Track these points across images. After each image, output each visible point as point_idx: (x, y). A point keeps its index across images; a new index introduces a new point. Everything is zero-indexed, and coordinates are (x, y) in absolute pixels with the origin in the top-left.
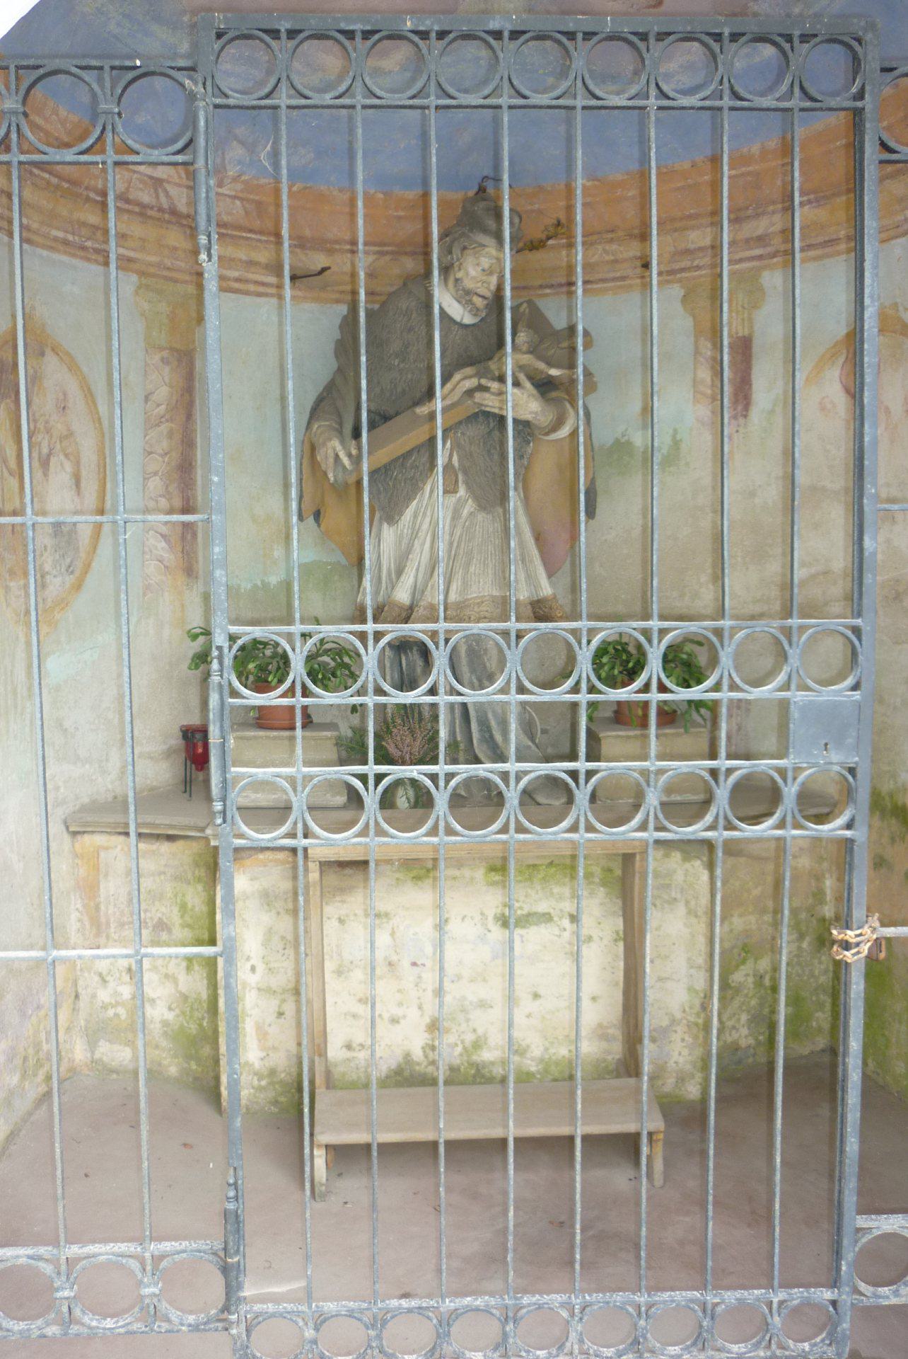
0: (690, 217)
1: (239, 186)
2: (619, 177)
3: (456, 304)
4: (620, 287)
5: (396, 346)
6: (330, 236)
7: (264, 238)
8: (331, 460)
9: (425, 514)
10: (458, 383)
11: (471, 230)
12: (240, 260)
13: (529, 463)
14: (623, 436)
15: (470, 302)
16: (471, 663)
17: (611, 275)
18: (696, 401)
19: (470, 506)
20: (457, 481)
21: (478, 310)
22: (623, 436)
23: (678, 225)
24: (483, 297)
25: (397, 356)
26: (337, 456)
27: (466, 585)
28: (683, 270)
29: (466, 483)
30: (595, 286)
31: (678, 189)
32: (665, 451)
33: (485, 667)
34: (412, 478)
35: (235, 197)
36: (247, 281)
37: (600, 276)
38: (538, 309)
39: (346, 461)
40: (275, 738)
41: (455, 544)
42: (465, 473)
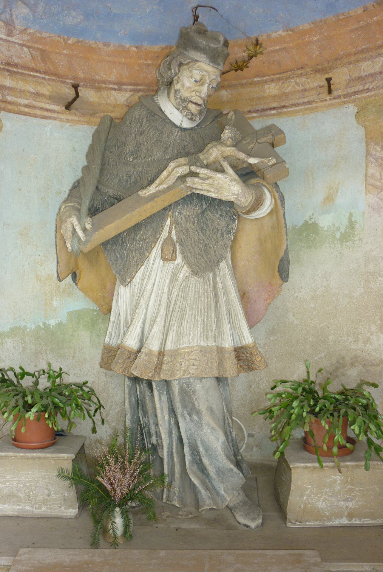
0: (362, 51)
1: (26, 37)
2: (307, 26)
3: (177, 112)
5: (130, 147)
6: (98, 77)
7: (47, 77)
8: (70, 233)
9: (149, 276)
10: (173, 170)
11: (186, 49)
12: (29, 92)
13: (235, 237)
14: (311, 219)
16: (183, 401)
17: (301, 101)
18: (367, 191)
19: (185, 271)
20: (174, 251)
21: (192, 114)
22: (311, 219)
23: (353, 58)
24: (196, 104)
25: (132, 154)
26: (74, 232)
27: (179, 336)
29: (182, 253)
30: (289, 109)
31: (352, 31)
32: (343, 230)
33: (194, 405)
34: (141, 249)
35: (23, 45)
36: (35, 107)
37: (294, 102)
39: (80, 234)
40: (22, 457)
41: (173, 302)
42: (181, 245)
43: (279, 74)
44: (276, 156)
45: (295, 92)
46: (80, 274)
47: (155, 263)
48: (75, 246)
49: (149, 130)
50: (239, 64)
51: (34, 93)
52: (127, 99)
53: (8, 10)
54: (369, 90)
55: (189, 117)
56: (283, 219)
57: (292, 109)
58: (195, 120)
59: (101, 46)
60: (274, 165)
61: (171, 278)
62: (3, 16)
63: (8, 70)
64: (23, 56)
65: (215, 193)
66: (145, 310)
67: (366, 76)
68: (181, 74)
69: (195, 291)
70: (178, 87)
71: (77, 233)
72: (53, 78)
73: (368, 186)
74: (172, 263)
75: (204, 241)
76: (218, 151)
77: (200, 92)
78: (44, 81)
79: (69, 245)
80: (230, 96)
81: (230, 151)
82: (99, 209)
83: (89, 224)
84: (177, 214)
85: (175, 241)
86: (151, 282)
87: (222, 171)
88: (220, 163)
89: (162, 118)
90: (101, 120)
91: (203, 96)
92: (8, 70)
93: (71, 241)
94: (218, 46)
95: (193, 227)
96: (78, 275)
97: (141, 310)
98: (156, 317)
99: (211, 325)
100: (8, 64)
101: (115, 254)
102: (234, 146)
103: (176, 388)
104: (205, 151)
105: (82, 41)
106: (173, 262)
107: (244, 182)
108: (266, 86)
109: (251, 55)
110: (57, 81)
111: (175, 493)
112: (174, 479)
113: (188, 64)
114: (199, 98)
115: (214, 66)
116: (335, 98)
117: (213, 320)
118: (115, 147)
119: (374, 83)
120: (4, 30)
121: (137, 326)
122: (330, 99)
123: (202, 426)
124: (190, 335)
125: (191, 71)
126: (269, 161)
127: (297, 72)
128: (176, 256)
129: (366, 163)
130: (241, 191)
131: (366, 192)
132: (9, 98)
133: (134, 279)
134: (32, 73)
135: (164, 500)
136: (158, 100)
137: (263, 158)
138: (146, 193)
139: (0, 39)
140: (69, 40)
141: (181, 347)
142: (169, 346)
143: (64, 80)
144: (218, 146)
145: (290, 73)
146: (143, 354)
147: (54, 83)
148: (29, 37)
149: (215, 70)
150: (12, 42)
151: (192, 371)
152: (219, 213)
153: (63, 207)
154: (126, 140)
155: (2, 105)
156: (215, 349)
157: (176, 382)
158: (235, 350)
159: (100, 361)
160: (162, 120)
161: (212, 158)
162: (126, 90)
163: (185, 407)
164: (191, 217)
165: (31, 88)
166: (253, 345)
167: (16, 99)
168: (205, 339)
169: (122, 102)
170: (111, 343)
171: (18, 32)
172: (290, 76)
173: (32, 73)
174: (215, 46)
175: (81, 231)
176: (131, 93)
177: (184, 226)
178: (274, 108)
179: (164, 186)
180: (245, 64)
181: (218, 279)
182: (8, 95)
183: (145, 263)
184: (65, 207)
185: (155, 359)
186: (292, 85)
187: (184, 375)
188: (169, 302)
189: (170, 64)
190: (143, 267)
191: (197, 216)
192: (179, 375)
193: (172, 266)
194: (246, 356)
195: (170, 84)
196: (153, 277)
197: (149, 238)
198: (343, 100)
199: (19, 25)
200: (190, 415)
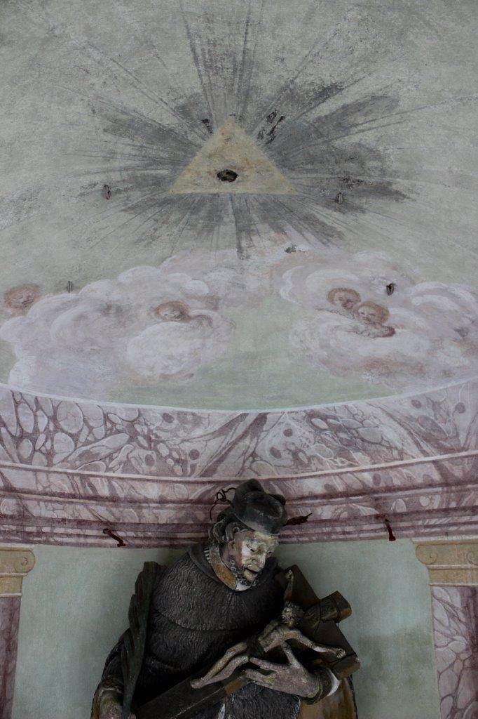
60: (343, 658)
81: (294, 634)
87: (283, 661)
144: (280, 630)
161: (272, 645)
189: (224, 527)
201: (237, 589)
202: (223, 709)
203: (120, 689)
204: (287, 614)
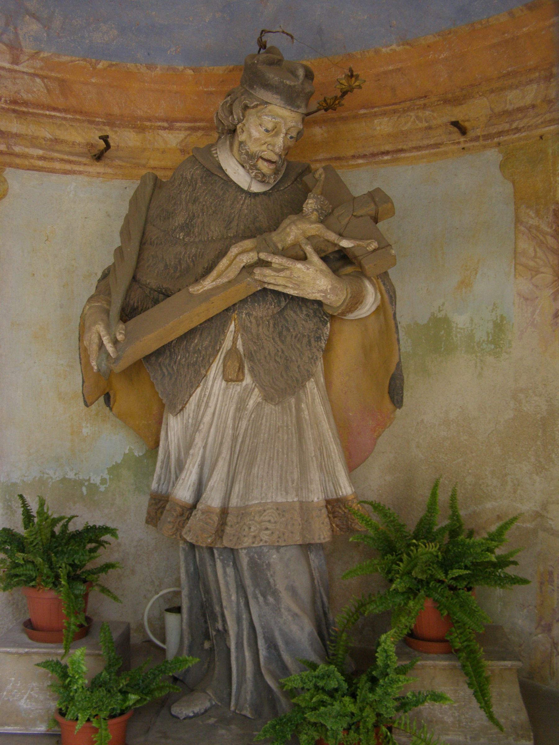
1: (38, 64)
3: (241, 170)
4: (435, 154)
6: (140, 113)
7: (69, 116)
8: (95, 347)
9: (207, 403)
14: (440, 311)
15: (255, 166)
17: (426, 142)
19: (256, 397)
20: (241, 368)
21: (264, 175)
26: (101, 345)
27: (247, 487)
28: (500, 134)
29: (252, 370)
30: (408, 155)
33: (269, 583)
36: (52, 159)
37: (415, 144)
38: (339, 181)
39: (109, 347)
41: (240, 440)
43: (394, 104)
44: (380, 238)
45: (416, 129)
46: (115, 395)
47: (215, 385)
48: (103, 365)
49: (206, 194)
50: (328, 101)
51: (51, 140)
52: (182, 141)
53: (11, 28)
54: (518, 130)
55: (259, 179)
56: (393, 322)
57: (412, 154)
58: (268, 183)
59: (143, 70)
60: (375, 250)
61: (237, 406)
62: (5, 37)
63: (14, 111)
64: (35, 90)
65: (294, 289)
66: (202, 450)
67: (513, 110)
68: (247, 121)
69: (270, 425)
70: (242, 137)
71: (105, 347)
72: (78, 117)
73: (518, 266)
74: (238, 385)
75: (283, 352)
76: (298, 229)
77: (274, 146)
78: (64, 122)
79: (94, 364)
80: (325, 135)
81: (314, 229)
82: (138, 307)
83: (121, 333)
84: (244, 316)
85: (242, 353)
86: (210, 411)
87: (303, 258)
88: (300, 246)
89: (222, 179)
90: (141, 180)
91: (277, 150)
92: (14, 111)
93: (98, 358)
94: (296, 83)
95: (267, 333)
96: (112, 396)
97: (197, 449)
98: (217, 460)
99: (292, 473)
100: (15, 102)
101: (161, 369)
102: (322, 222)
103: (244, 561)
104: (280, 229)
105: (117, 64)
106: (240, 383)
107: (335, 271)
108: (376, 121)
109: (345, 90)
110: (84, 121)
111: (246, 699)
112: (245, 680)
113: (256, 106)
114: (272, 153)
115: (293, 109)
116: (471, 140)
117: (295, 464)
118: (160, 219)
119: (526, 121)
120: (8, 57)
121: (191, 472)
122: (465, 142)
123: (280, 611)
124: (262, 487)
125: (260, 117)
126: (368, 245)
127: (418, 102)
128: (243, 374)
129: (515, 234)
130: (330, 287)
131: (515, 275)
132: (17, 149)
133: (188, 405)
134: (48, 113)
135: (232, 708)
136: (217, 153)
137: (361, 239)
138: (198, 290)
139: (3, 68)
140: (98, 64)
141: (250, 503)
142: (234, 502)
143: (93, 119)
145: (408, 104)
146: (200, 512)
147: (78, 124)
148: (42, 64)
149: (293, 115)
150: (19, 71)
151: (265, 538)
152: (305, 313)
153: (88, 307)
154: (175, 210)
155: (7, 159)
156: (297, 505)
157: (243, 551)
158: (328, 502)
159: (146, 516)
160: (222, 181)
161: (290, 239)
162: (179, 129)
163: (256, 585)
164: (264, 319)
165: (47, 133)
166: (353, 497)
167: (27, 150)
168: (284, 493)
169: (174, 145)
170: (160, 490)
171: (26, 58)
172: (408, 108)
173: (48, 113)
174: (292, 84)
175: (110, 345)
176: (188, 132)
177: (254, 331)
178: (387, 153)
179: (220, 281)
180: (337, 102)
181: (303, 406)
182: (15, 145)
183: (201, 384)
184: (89, 309)
185: (216, 519)
186: (412, 119)
187: (253, 543)
188: (235, 438)
190: (199, 390)
191: (273, 317)
192: (247, 542)
193: (239, 388)
194: (343, 511)
195: (233, 132)
196: (212, 404)
197: (206, 349)
198: (482, 142)
199: (28, 48)
200: (264, 596)
201: (251, 189)
202: (232, 327)
203: (107, 304)
204: (309, 206)
